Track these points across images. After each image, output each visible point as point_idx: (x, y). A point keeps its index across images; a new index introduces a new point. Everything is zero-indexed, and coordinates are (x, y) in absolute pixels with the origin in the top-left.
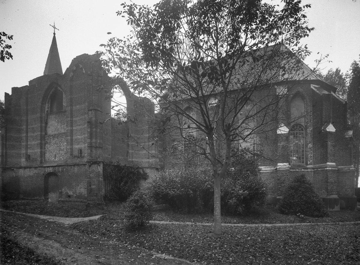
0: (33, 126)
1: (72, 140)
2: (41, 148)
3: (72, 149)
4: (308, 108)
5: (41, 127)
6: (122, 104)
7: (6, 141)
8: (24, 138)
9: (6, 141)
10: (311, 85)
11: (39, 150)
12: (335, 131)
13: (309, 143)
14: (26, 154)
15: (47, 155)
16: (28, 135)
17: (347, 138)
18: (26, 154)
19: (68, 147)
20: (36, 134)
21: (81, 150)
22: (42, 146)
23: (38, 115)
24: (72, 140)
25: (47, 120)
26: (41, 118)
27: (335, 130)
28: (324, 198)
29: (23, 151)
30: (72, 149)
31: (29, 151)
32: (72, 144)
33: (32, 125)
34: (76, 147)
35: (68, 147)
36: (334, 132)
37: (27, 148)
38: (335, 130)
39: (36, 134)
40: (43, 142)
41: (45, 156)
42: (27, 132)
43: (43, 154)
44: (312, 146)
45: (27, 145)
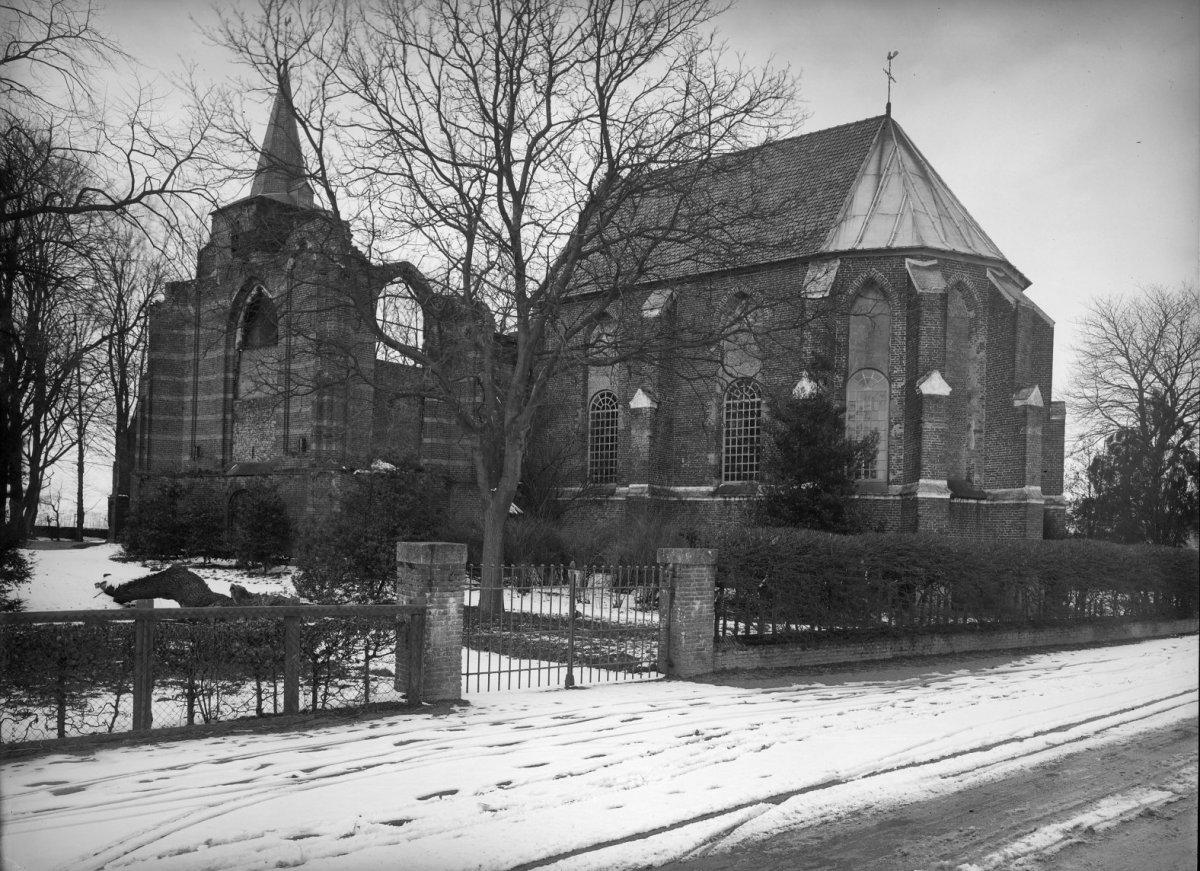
0: (210, 378)
1: (287, 415)
2: (224, 431)
3: (286, 437)
4: (895, 326)
5: (226, 380)
6: (570, 130)
7: (150, 413)
8: (189, 406)
9: (150, 413)
10: (907, 260)
11: (220, 437)
12: (947, 394)
13: (896, 424)
14: (193, 442)
15: (238, 448)
16: (199, 399)
17: (1016, 409)
18: (193, 442)
19: (278, 432)
20: (214, 397)
21: (304, 440)
22: (226, 427)
23: (220, 352)
24: (287, 415)
25: (239, 363)
26: (227, 358)
27: (951, 389)
28: (1185, 617)
29: (187, 438)
30: (286, 437)
31: (200, 437)
32: (287, 426)
33: (206, 375)
34: (295, 432)
35: (278, 432)
36: (946, 397)
37: (194, 431)
38: (951, 389)
39: (214, 397)
40: (229, 417)
41: (231, 450)
42: (195, 394)
43: (227, 446)
44: (902, 431)
45: (194, 423)
